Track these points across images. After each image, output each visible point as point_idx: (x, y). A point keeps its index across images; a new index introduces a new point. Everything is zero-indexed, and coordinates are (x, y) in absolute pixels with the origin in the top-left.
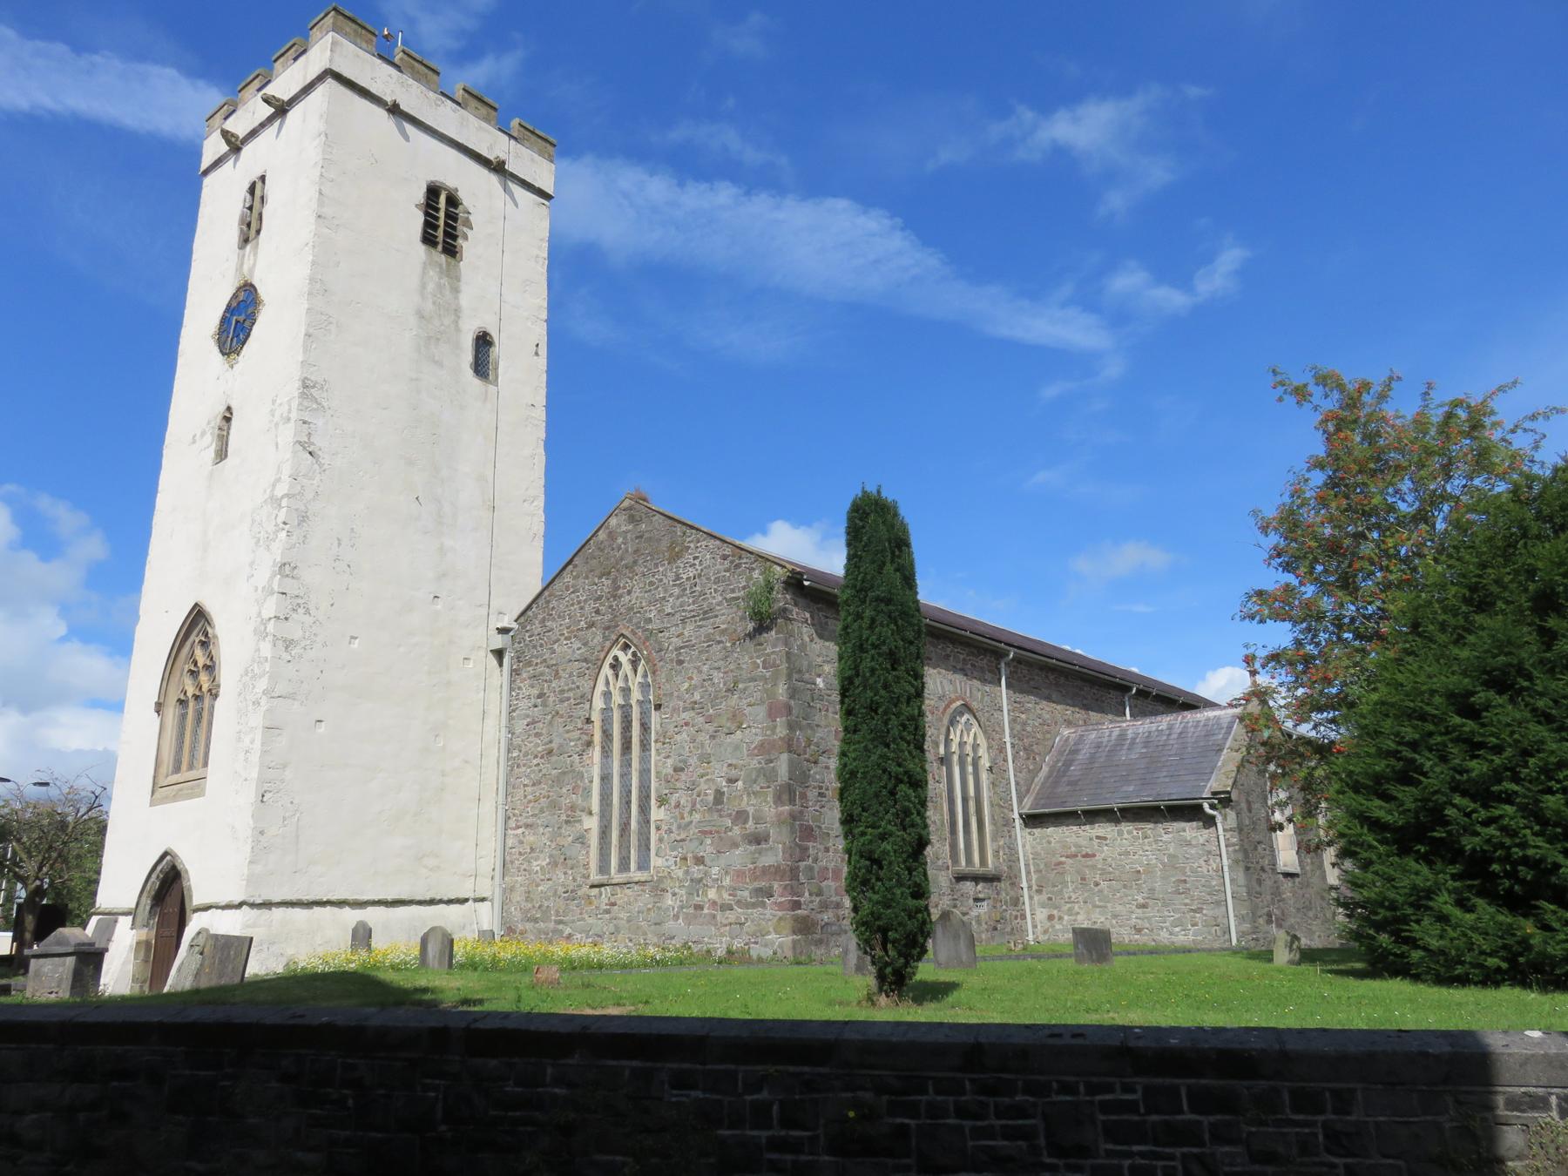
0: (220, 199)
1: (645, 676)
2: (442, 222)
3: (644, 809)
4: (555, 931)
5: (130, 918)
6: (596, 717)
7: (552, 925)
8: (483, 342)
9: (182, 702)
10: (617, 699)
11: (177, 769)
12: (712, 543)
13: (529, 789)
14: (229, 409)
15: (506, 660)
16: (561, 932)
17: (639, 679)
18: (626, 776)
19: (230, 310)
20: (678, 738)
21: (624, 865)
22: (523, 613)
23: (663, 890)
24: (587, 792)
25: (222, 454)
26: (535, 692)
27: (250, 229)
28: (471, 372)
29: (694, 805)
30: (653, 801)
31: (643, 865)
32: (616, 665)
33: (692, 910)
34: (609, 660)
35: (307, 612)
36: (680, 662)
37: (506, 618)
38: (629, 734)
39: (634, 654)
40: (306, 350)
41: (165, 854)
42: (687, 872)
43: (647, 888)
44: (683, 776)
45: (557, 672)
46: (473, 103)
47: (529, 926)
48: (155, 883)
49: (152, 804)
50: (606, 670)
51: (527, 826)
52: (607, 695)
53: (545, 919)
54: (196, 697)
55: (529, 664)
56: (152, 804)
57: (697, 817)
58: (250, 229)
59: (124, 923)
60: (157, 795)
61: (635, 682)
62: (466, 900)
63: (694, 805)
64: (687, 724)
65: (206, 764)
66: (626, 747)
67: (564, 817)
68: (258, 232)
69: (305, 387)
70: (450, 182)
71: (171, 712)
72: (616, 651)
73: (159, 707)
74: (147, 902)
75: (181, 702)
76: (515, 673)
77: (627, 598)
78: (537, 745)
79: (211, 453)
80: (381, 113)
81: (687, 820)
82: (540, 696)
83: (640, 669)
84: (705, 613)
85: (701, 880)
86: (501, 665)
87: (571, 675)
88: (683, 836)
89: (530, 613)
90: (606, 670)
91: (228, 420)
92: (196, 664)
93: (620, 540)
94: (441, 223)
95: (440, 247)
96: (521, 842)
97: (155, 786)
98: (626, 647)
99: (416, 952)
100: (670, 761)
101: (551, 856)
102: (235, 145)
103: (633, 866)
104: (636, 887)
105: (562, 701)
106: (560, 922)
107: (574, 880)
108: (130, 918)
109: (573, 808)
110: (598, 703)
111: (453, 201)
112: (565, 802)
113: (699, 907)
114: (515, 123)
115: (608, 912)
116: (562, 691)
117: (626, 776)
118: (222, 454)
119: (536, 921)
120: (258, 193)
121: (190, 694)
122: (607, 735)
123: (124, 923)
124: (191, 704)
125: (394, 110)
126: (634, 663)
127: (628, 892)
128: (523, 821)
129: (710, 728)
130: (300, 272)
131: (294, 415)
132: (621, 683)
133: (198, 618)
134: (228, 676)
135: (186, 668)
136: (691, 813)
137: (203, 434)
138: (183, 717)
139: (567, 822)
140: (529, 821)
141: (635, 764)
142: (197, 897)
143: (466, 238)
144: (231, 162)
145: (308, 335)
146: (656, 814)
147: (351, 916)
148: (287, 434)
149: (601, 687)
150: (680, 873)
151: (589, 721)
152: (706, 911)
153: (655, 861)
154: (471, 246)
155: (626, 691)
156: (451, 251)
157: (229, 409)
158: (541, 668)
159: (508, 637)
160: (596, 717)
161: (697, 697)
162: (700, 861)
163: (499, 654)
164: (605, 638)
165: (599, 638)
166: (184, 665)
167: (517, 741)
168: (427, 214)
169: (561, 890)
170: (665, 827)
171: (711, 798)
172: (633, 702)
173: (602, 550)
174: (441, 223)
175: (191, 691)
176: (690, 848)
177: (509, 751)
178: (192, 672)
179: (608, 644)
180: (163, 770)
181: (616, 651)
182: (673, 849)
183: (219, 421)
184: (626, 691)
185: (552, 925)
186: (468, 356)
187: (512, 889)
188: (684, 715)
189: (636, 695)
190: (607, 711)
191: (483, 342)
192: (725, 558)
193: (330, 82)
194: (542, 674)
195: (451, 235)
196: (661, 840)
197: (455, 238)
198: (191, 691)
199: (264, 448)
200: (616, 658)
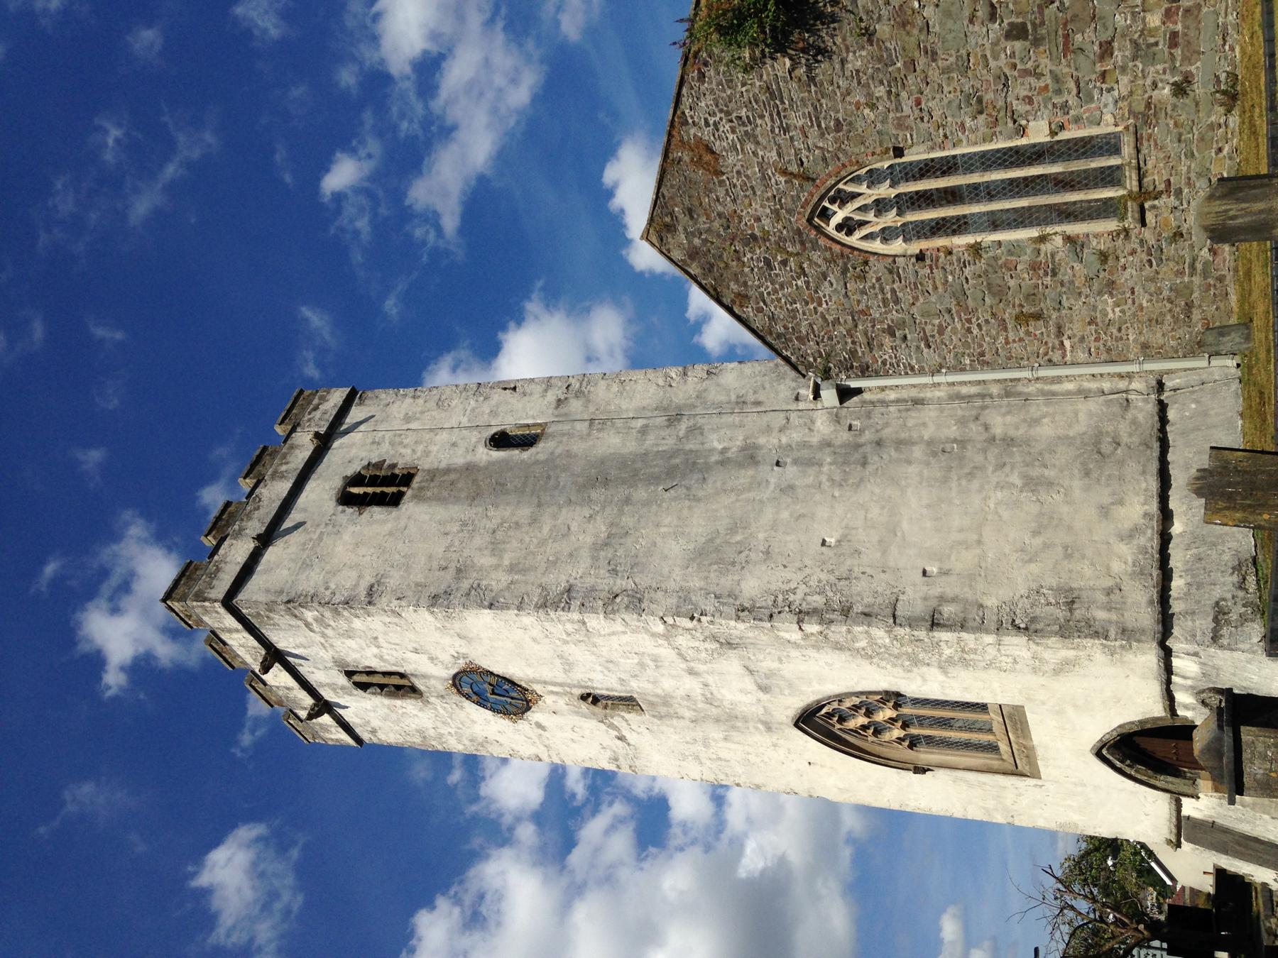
0: (374, 717)
1: (857, 180)
2: (379, 488)
3: (1037, 154)
4: (1205, 274)
5: (1185, 800)
6: (915, 247)
7: (1197, 280)
8: (501, 440)
9: (913, 743)
10: (891, 218)
11: (992, 748)
12: (686, 101)
13: (1011, 336)
14: (584, 698)
15: (854, 384)
16: (1206, 264)
17: (863, 188)
18: (991, 191)
19: (481, 701)
20: (937, 114)
21: (1109, 177)
22: (794, 367)
23: (1148, 105)
24: (1015, 248)
25: (629, 702)
26: (887, 340)
27: (398, 685)
28: (532, 450)
29: (1026, 73)
30: (1023, 141)
31: (1110, 145)
32: (848, 226)
33: (1178, 52)
34: (841, 236)
35: (794, 591)
36: (838, 125)
37: (803, 392)
38: (934, 194)
39: (832, 201)
40: (506, 607)
41: (1099, 754)
42: (1124, 69)
43: (1145, 132)
44: (989, 96)
45: (862, 312)
46: (259, 468)
47: (1196, 314)
48: (1140, 771)
49: (1035, 774)
50: (854, 240)
51: (1060, 332)
52: (887, 235)
53: (1189, 287)
54: (905, 726)
55: (853, 353)
56: (1035, 774)
57: (1046, 64)
58: (398, 685)
59: (1190, 808)
60: (1026, 770)
61: (870, 194)
62: (1161, 402)
63: (1026, 73)
64: (918, 103)
65: (983, 707)
66: (952, 196)
67: (1048, 280)
68: (402, 676)
69: (544, 606)
70: (338, 483)
71: (924, 755)
72: (831, 228)
73: (920, 770)
74: (1162, 780)
75: (912, 746)
76: (865, 371)
77: (766, 222)
78: (954, 331)
79: (632, 716)
80: (271, 554)
81: (1048, 80)
82: (891, 332)
83: (850, 188)
84: (772, 94)
85: (1135, 44)
86: (859, 391)
87: (864, 292)
88: (1072, 85)
89: (793, 359)
90: (854, 240)
91: (596, 700)
92: (864, 728)
93: (697, 241)
94: (378, 490)
95: (404, 489)
96: (1082, 339)
97: (1016, 773)
98: (825, 215)
99: (1168, 795)
100: (969, 123)
101: (1100, 293)
102: (323, 706)
103: (1114, 161)
104: (1144, 151)
105: (897, 301)
106: (1192, 266)
107: (1133, 252)
108: (1185, 800)
109: (1034, 267)
110: (897, 246)
111: (357, 480)
112: (1027, 279)
113: (1173, 39)
114: (280, 430)
115: (1179, 192)
116: (885, 301)
117: (991, 191)
118: (629, 702)
119: (1189, 306)
120: (364, 679)
121: (901, 733)
122: (938, 228)
123: (1190, 808)
124: (914, 731)
125: (265, 540)
126: (843, 199)
127: (1150, 165)
128: (1053, 341)
129: (922, 62)
130: (424, 622)
131: (576, 616)
132: (870, 216)
133: (814, 721)
134: (877, 678)
135: (871, 738)
136: (1039, 76)
137: (612, 726)
138: (930, 740)
139: (1054, 274)
140: (1053, 330)
141: (975, 178)
142: (1155, 709)
143: (394, 466)
144: (341, 711)
145: (491, 606)
146: (1038, 133)
147: (1187, 513)
148: (596, 622)
149: (877, 246)
150: (1124, 80)
151: (920, 257)
152: (1179, 27)
153: (1107, 127)
154: (403, 457)
155: (880, 206)
156: (407, 479)
157: (584, 698)
158: (860, 337)
159: (823, 385)
160: (915, 247)
161: (880, 91)
162: (1107, 50)
163: (845, 394)
164: (815, 246)
165: (815, 256)
166: (870, 742)
167: (950, 359)
168: (369, 504)
169: (1148, 271)
170: (1061, 118)
171: (1018, 45)
172: (893, 193)
173: (712, 266)
174: (378, 490)
175: (897, 732)
176: (1088, 70)
177: (963, 370)
178: (877, 732)
179: (822, 241)
180: (996, 764)
181: (831, 228)
182: (1091, 99)
183: (598, 709)
184: (880, 206)
185: (1197, 280)
186: (515, 453)
187: (1145, 346)
188: (907, 110)
189: (885, 190)
190: (908, 232)
191: (501, 440)
192: (702, 76)
193: (242, 598)
194: (866, 333)
195: (391, 480)
196: (1077, 120)
197: (394, 476)
198: (897, 732)
199: (614, 649)
200: (839, 228)
